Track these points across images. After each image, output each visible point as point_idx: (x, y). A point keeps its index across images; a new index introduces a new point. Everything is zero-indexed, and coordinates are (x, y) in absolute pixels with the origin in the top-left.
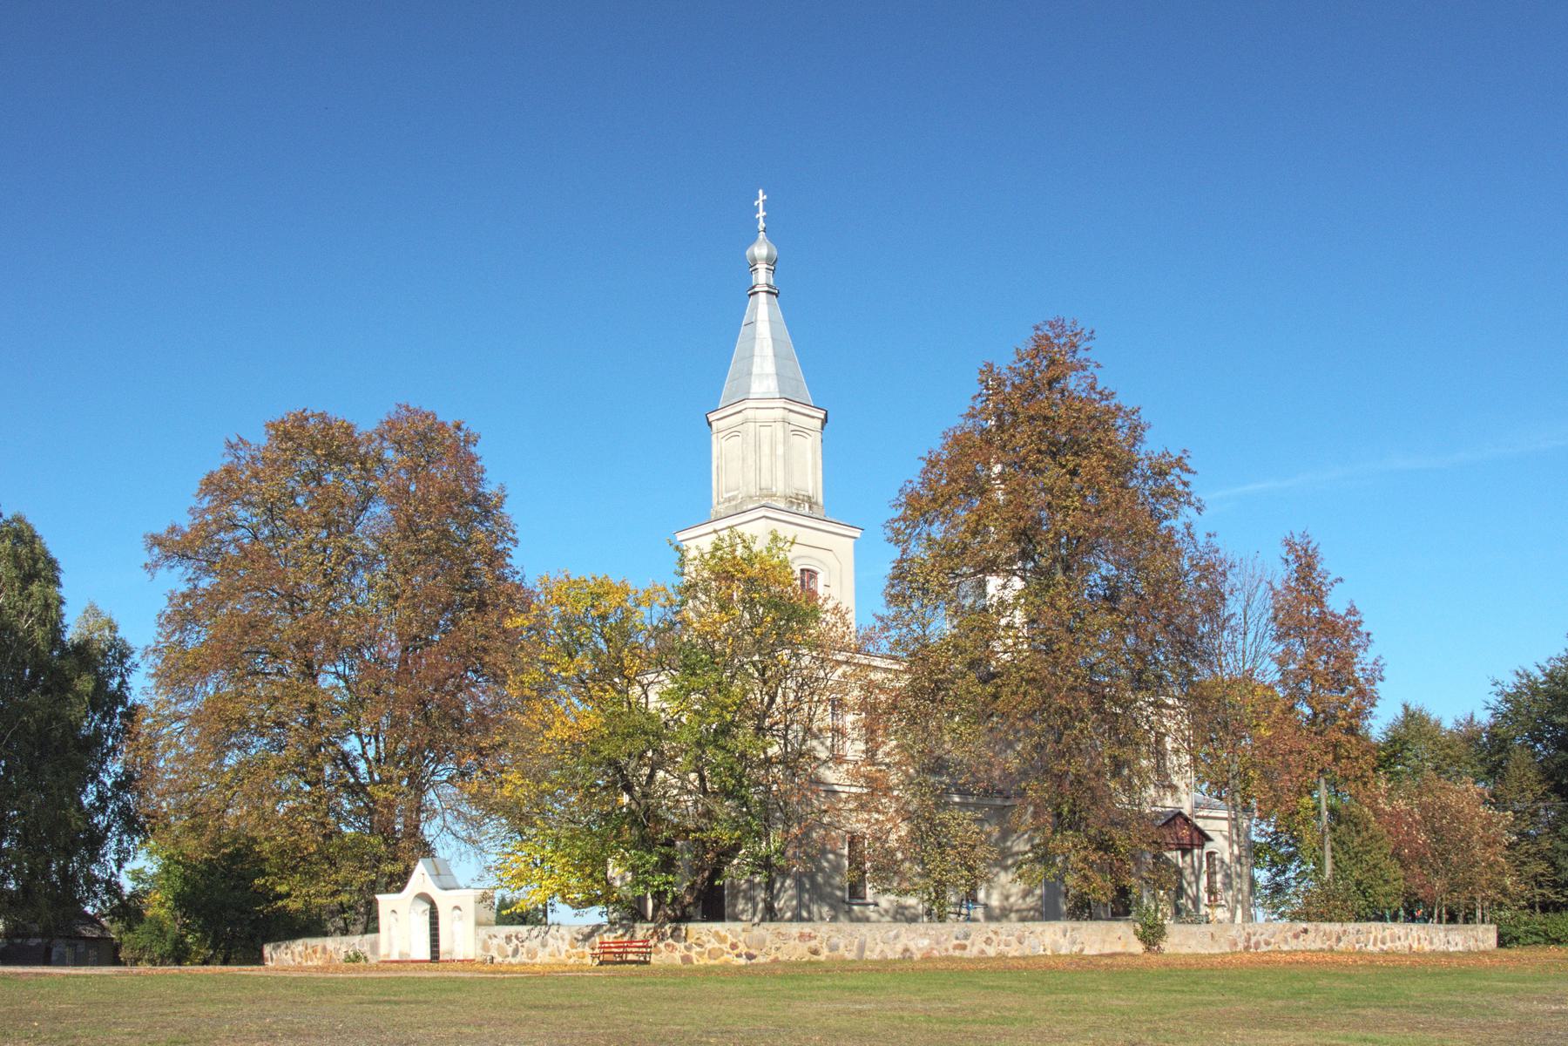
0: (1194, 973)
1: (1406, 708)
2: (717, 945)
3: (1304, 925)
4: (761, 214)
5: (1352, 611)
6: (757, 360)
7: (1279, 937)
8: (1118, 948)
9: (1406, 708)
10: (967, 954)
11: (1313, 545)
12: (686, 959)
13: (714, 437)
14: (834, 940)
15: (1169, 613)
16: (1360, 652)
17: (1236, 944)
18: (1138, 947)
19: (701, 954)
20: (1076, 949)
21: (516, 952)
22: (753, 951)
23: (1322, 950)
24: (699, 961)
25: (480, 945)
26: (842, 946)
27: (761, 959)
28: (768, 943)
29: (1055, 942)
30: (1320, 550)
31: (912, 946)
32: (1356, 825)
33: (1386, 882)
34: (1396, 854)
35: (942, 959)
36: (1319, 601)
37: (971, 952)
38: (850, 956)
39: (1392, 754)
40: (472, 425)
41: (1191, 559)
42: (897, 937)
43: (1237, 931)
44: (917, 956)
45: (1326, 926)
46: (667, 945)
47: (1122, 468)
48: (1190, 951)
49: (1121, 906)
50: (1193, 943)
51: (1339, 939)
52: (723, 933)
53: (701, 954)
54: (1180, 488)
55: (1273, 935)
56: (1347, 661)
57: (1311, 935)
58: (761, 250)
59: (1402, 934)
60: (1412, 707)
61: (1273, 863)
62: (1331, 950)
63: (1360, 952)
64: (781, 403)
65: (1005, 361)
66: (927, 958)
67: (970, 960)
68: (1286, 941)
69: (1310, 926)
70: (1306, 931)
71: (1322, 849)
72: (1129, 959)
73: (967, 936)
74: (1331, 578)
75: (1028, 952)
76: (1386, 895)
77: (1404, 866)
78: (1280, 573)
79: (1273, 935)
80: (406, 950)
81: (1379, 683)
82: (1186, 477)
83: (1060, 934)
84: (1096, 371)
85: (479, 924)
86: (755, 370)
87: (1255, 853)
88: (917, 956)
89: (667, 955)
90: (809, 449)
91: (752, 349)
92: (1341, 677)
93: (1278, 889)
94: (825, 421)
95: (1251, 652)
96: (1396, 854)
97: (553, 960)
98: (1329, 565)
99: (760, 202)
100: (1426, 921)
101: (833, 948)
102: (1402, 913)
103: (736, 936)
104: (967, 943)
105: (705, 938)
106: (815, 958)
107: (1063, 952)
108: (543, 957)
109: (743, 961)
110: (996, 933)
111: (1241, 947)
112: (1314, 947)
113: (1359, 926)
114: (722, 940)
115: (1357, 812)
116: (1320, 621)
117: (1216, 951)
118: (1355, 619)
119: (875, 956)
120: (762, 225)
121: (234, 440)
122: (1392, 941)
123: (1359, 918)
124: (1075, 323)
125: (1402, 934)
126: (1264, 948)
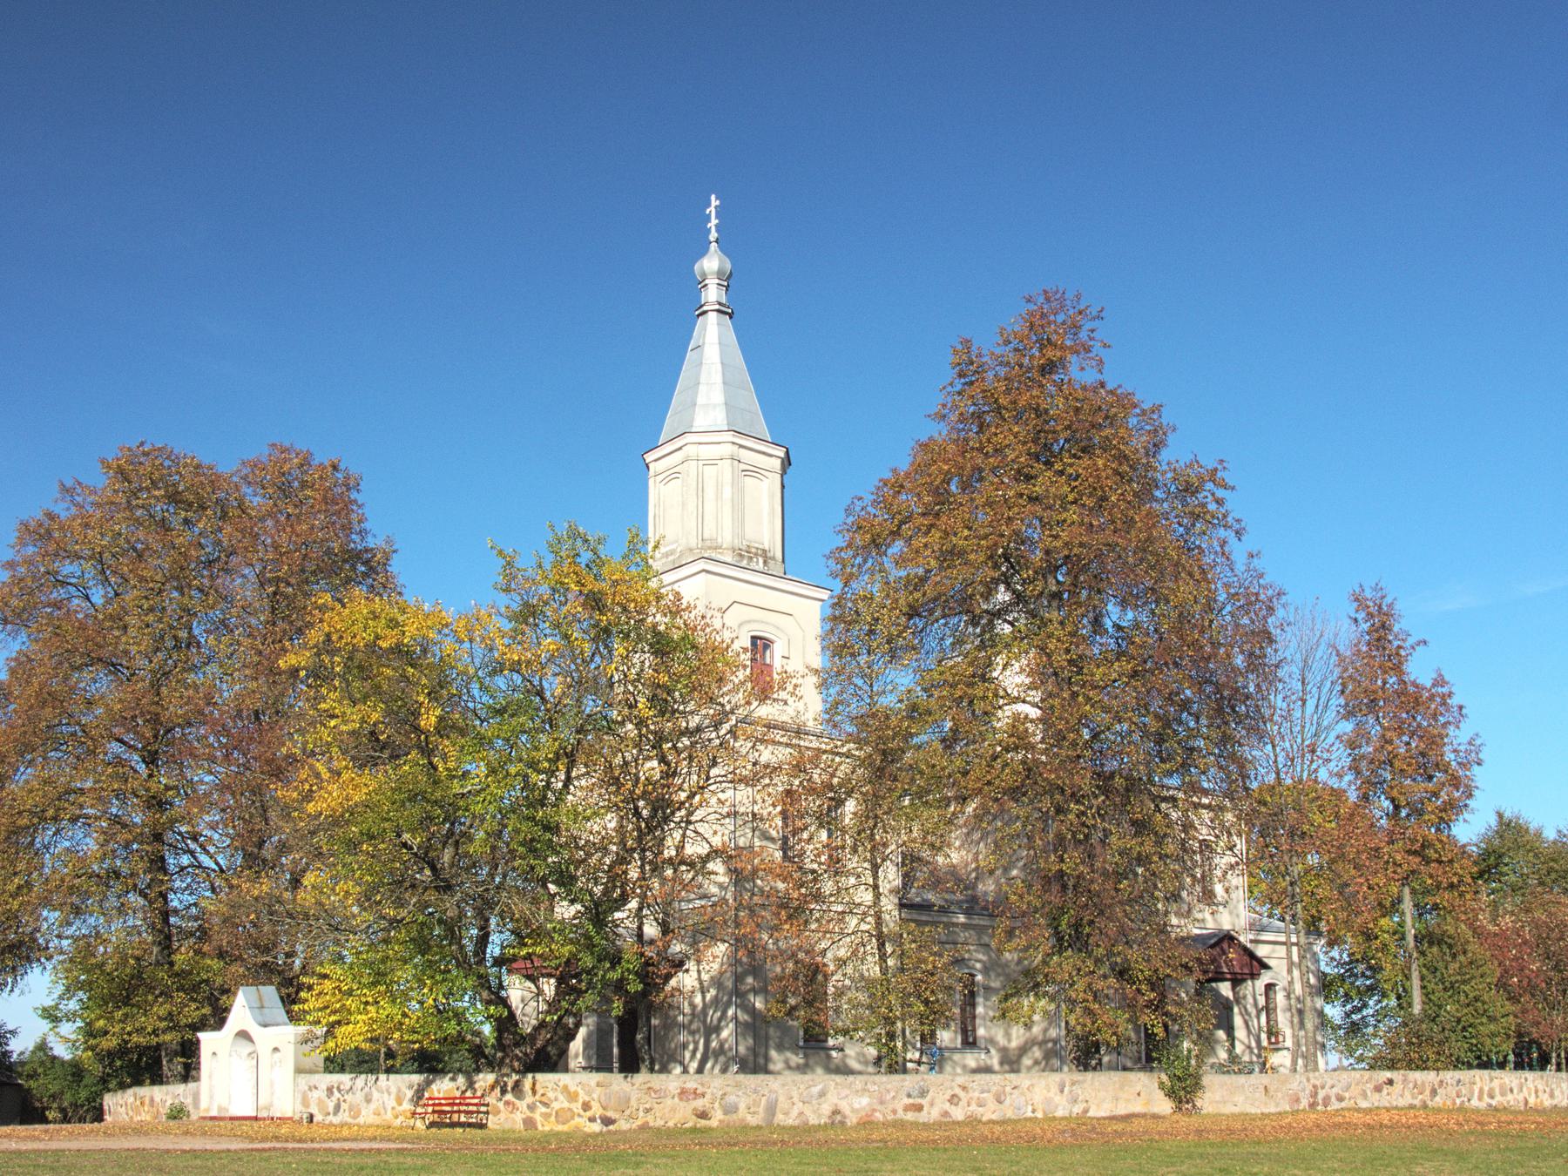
0: (1242, 1137)
1: (1500, 816)
2: (566, 1105)
3: (1388, 1074)
4: (714, 221)
5: (1440, 681)
6: (702, 388)
7: (1355, 1091)
8: (1138, 1108)
9: (1500, 816)
10: (923, 1117)
11: (1388, 600)
12: (530, 1123)
13: (651, 482)
14: (731, 1099)
15: (1204, 684)
16: (1451, 730)
17: (1298, 1100)
18: (1164, 1106)
19: (546, 1116)
20: (1077, 1109)
21: (337, 1108)
22: (610, 1114)
23: (1412, 1107)
24: (545, 1126)
25: (299, 1100)
26: (742, 1106)
27: (622, 1125)
28: (633, 1103)
29: (1048, 1101)
30: (1398, 606)
31: (844, 1106)
32: (1450, 947)
33: (1492, 1019)
34: (1502, 985)
35: (885, 1125)
36: (1398, 669)
37: (931, 1114)
38: (753, 1120)
39: (1489, 863)
40: (352, 464)
41: (1227, 586)
42: (822, 1094)
43: (1300, 1084)
44: (852, 1120)
45: (1417, 1076)
46: (507, 1103)
47: (1135, 472)
48: (1236, 1110)
49: (1150, 1053)
50: (1239, 1099)
51: (1434, 1092)
52: (572, 1089)
53: (546, 1116)
54: (1212, 507)
55: (1348, 1088)
56: (1435, 741)
57: (1398, 1087)
58: (712, 263)
59: (1515, 1085)
60: (1508, 815)
61: (1347, 998)
62: (1425, 1106)
63: (1461, 1109)
64: (729, 437)
65: (988, 344)
66: (866, 1123)
67: (926, 1126)
68: (1364, 1095)
69: (1395, 1075)
70: (1390, 1082)
71: (1408, 977)
72: (1150, 1124)
73: (923, 1093)
74: (1411, 641)
75: (1010, 1114)
76: (1493, 1035)
77: (1514, 999)
78: (1346, 632)
79: (1348, 1088)
80: (225, 1104)
81: (1475, 767)
82: (1220, 493)
83: (1055, 1089)
84: (1103, 353)
85: (299, 1070)
86: (700, 400)
87: (1326, 987)
88: (852, 1120)
89: (506, 1116)
90: (765, 493)
91: (698, 374)
92: (1428, 762)
93: (1354, 1029)
94: (787, 462)
95: (1309, 738)
96: (1502, 985)
97: (377, 1120)
98: (1409, 622)
99: (712, 210)
100: (1543, 1068)
101: (730, 1110)
102: (1511, 1057)
103: (589, 1093)
104: (924, 1102)
105: (551, 1095)
106: (703, 1123)
107: (1060, 1113)
108: (367, 1116)
109: (596, 1127)
110: (964, 1088)
111: (1304, 1103)
112: (1402, 1102)
113: (1458, 1074)
114: (573, 1097)
115: (1451, 931)
116: (1399, 694)
117: (1273, 1109)
118: (1445, 690)
119: (790, 1121)
120: (713, 235)
121: (69, 483)
122: (1503, 1094)
123: (1458, 1064)
124: (1079, 297)
125: (1515, 1085)
126: (1335, 1105)
